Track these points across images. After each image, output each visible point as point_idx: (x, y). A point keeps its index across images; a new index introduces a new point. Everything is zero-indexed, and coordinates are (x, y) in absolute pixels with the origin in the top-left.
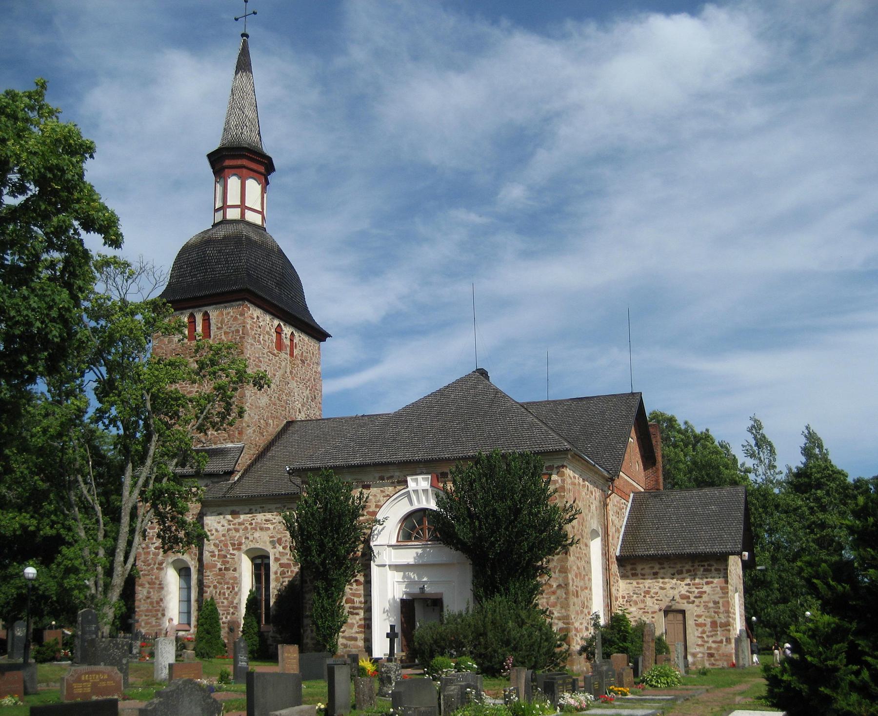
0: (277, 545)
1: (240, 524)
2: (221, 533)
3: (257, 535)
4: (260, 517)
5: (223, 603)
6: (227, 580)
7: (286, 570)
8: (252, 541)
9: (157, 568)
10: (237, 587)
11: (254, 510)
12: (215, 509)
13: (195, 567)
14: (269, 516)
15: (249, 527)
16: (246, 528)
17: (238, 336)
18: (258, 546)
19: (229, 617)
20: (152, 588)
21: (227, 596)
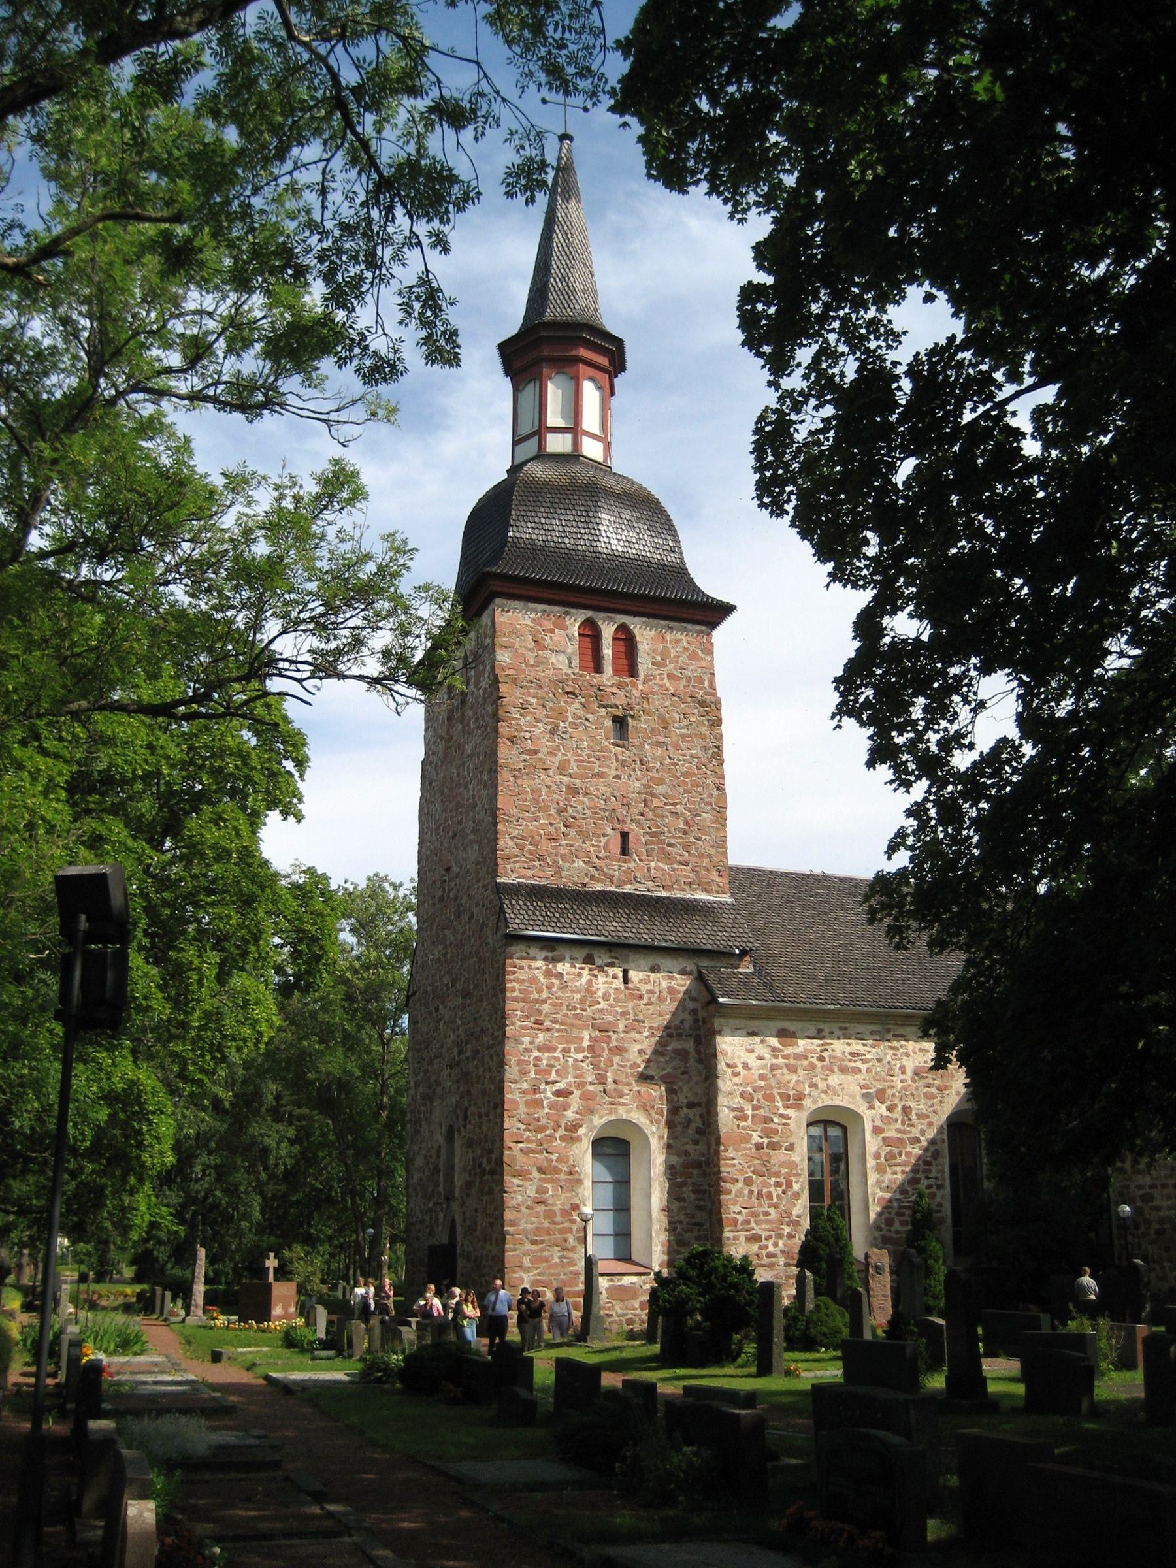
0: (877, 1103)
1: (797, 1057)
2: (756, 1073)
3: (835, 1080)
4: (840, 1047)
5: (767, 1214)
6: (776, 1168)
7: (896, 1150)
8: (825, 1092)
9: (562, 1138)
10: (797, 1182)
11: (826, 1033)
12: (743, 1022)
13: (660, 1138)
14: (857, 1046)
15: (818, 1064)
16: (812, 1067)
17: (701, 688)
18: (838, 1102)
19: (781, 1243)
20: (550, 1181)
21: (775, 1200)
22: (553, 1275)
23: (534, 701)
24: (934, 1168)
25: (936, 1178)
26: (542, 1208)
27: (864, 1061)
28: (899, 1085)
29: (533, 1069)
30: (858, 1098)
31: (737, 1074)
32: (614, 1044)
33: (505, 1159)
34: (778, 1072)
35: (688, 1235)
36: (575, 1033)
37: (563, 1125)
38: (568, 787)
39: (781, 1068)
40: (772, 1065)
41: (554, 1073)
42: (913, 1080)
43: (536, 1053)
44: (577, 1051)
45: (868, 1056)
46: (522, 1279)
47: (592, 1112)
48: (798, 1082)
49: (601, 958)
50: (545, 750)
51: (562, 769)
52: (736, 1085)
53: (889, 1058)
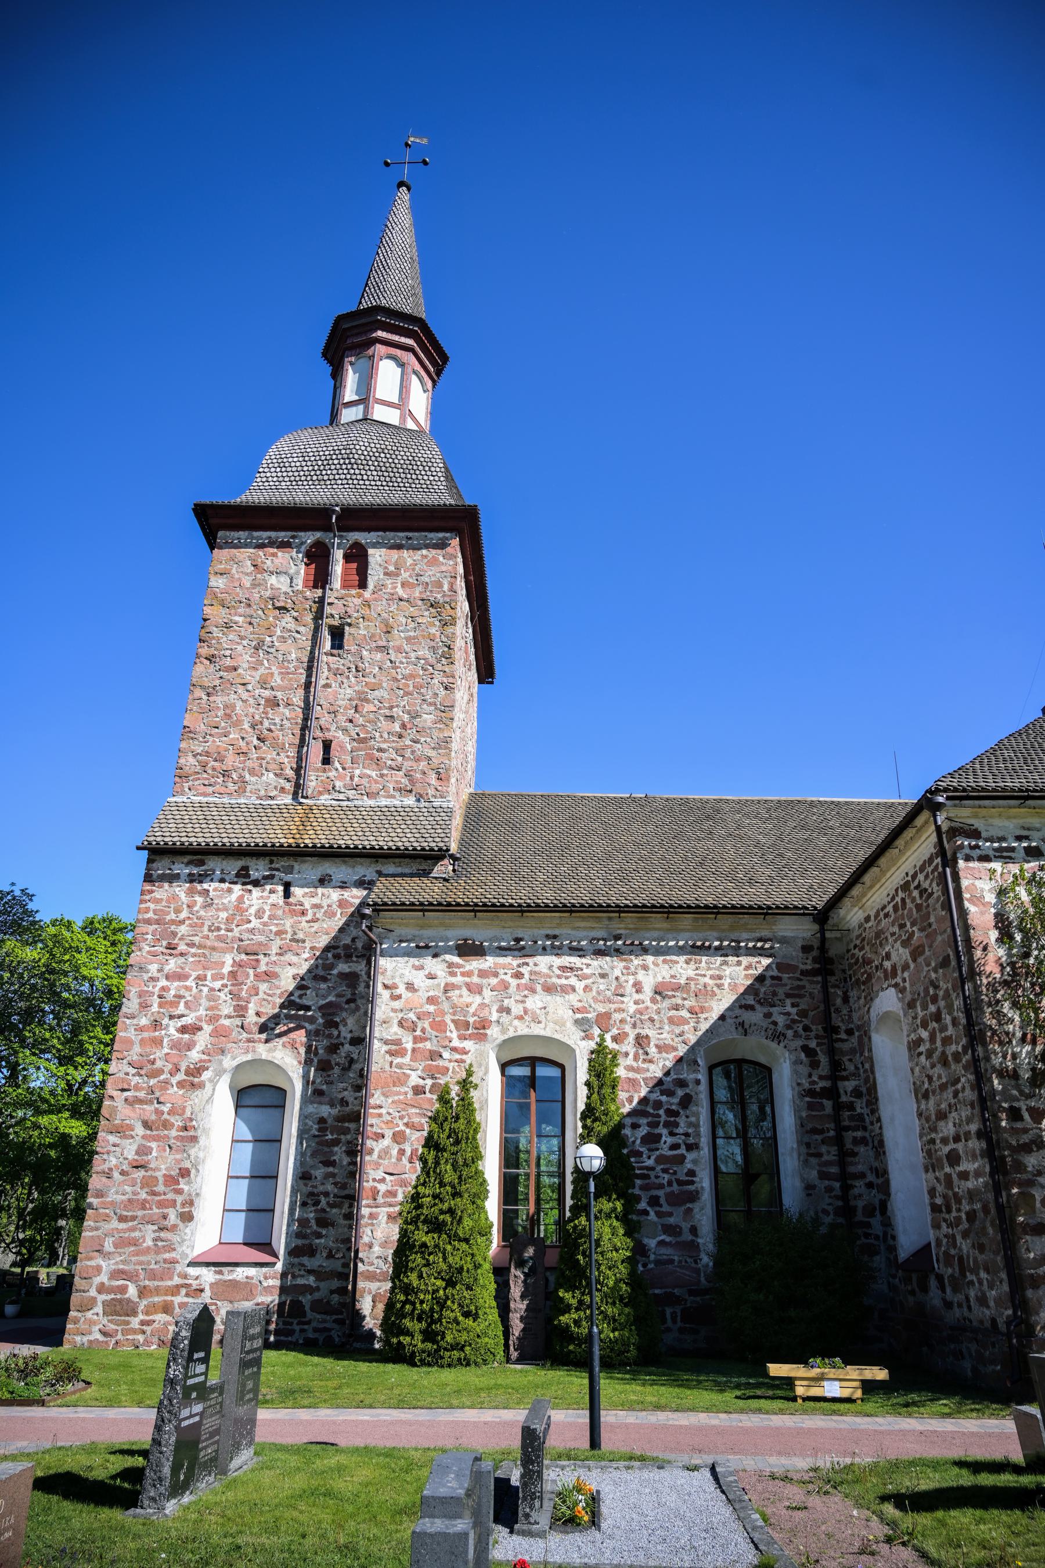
1: (483, 974)
2: (423, 995)
3: (535, 1002)
8: (520, 1018)
9: (181, 1084)
15: (514, 982)
18: (537, 1030)
22: (140, 1263)
23: (240, 619)
24: (682, 1121)
25: (687, 1135)
26: (141, 1173)
27: (580, 978)
28: (632, 1008)
29: (156, 1001)
30: (569, 1024)
31: (396, 998)
32: (263, 968)
33: (104, 1111)
34: (454, 994)
35: (334, 1210)
36: (216, 957)
37: (183, 1069)
38: (267, 700)
39: (459, 988)
40: (447, 985)
41: (182, 1005)
42: (653, 1001)
43: (164, 982)
44: (214, 978)
45: (586, 971)
46: (99, 1269)
47: (223, 1052)
48: (483, 1006)
49: (258, 869)
50: (245, 665)
51: (263, 684)
52: (394, 1011)
53: (617, 972)
